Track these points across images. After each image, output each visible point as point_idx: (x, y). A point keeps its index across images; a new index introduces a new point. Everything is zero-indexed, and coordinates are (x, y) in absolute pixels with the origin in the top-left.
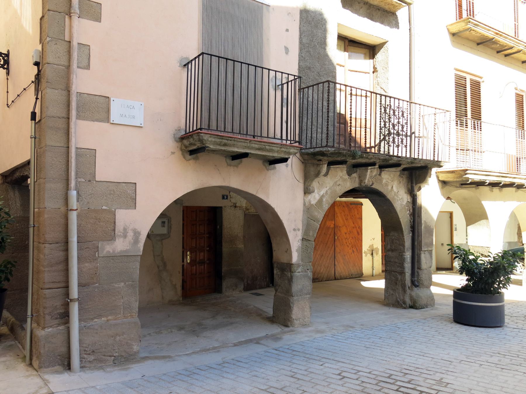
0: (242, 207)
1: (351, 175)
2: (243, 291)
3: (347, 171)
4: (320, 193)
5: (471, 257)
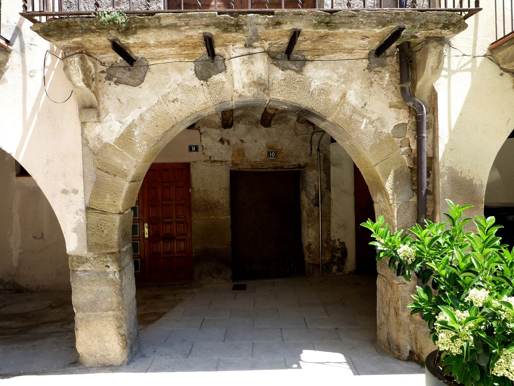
0: (226, 161)
1: (210, 76)
2: (231, 281)
3: (195, 70)
4: (123, 120)
5: (448, 276)
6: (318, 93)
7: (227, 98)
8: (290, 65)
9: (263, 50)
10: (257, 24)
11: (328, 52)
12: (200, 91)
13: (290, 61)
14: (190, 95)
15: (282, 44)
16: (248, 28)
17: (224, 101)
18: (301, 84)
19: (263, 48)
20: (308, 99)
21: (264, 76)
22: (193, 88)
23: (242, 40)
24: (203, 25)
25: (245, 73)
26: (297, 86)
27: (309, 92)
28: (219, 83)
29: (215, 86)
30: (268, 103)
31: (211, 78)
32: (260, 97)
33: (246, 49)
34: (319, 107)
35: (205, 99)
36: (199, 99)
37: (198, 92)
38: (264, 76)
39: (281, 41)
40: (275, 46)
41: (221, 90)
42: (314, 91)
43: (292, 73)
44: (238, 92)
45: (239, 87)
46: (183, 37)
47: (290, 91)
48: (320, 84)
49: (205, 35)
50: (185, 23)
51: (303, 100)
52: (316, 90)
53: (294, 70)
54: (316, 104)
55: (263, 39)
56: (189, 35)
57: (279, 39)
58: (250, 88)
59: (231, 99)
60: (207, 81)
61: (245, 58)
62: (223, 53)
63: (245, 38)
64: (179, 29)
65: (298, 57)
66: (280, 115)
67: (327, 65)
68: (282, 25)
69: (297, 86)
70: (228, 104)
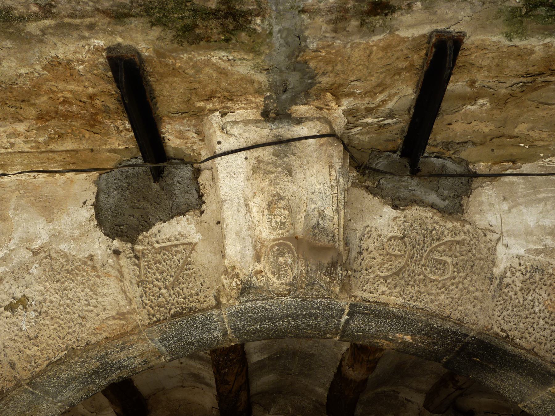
1: (147, 225)
3: (96, 206)
6: (523, 282)
7: (202, 299)
8: (419, 193)
9: (326, 130)
10: (303, 11)
11: (546, 148)
12: (108, 275)
13: (420, 177)
14: (72, 285)
15: (390, 115)
16: (270, 25)
17: (190, 309)
18: (460, 252)
19: (328, 122)
20: (488, 303)
21: (332, 220)
22: (85, 263)
23: (252, 91)
24: (105, 13)
25: (264, 205)
26: (449, 260)
27: (491, 279)
28: (174, 249)
29: (159, 257)
30: (347, 322)
31: (147, 231)
32: (317, 297)
33: (269, 124)
34: (531, 330)
35: (124, 302)
36: (100, 299)
37: (99, 277)
38: (332, 220)
39: (391, 97)
40: (369, 120)
41: (182, 270)
42: (509, 274)
43: (428, 214)
44: (238, 274)
45: (243, 257)
46: (38, 68)
47: (422, 277)
48: (528, 251)
49: (114, 54)
50: (40, 7)
51: (470, 307)
52: (513, 274)
53: (432, 206)
54: (516, 319)
55: (327, 90)
56: (61, 56)
57: (382, 87)
58: (281, 259)
59: (214, 303)
60: (133, 241)
61: (265, 153)
62: (193, 150)
63: (262, 78)
64: (19, 30)
65: (443, 166)
66: (379, 390)
67: (544, 192)
68: (395, 15)
69: (449, 260)
70: (208, 323)
